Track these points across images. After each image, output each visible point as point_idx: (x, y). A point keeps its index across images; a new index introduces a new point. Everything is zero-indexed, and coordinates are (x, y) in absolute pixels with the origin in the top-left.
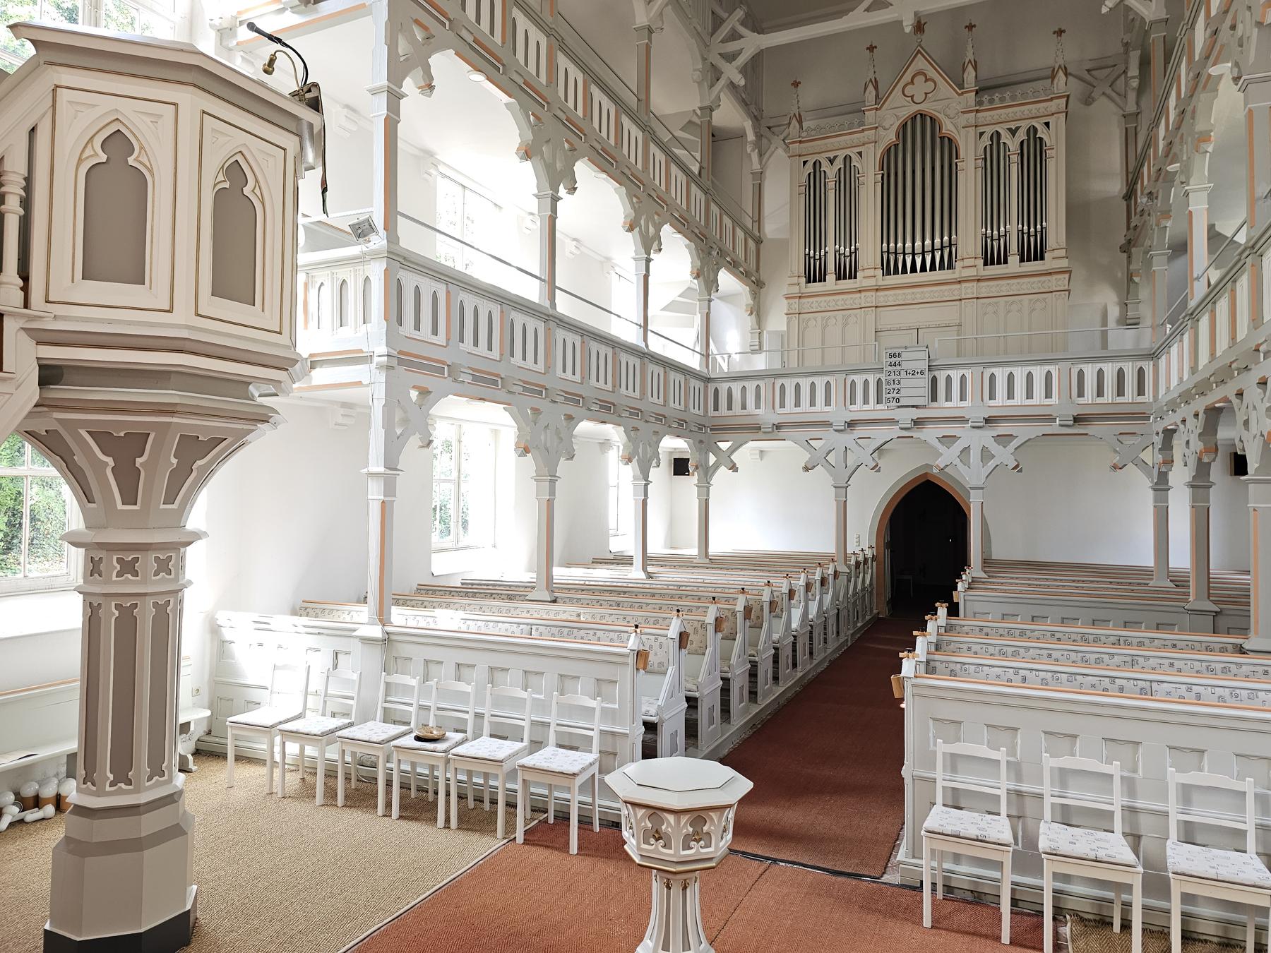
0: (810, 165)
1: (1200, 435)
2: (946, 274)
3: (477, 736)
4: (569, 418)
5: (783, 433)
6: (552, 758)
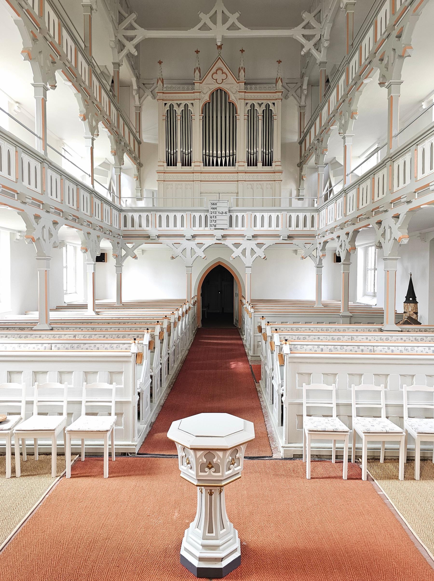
0: (168, 105)
1: (349, 242)
2: (231, 168)
3: (29, 415)
4: (55, 223)
5: (161, 240)
6: (84, 423)
